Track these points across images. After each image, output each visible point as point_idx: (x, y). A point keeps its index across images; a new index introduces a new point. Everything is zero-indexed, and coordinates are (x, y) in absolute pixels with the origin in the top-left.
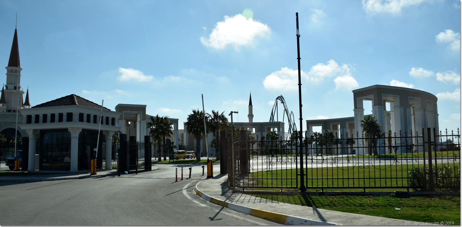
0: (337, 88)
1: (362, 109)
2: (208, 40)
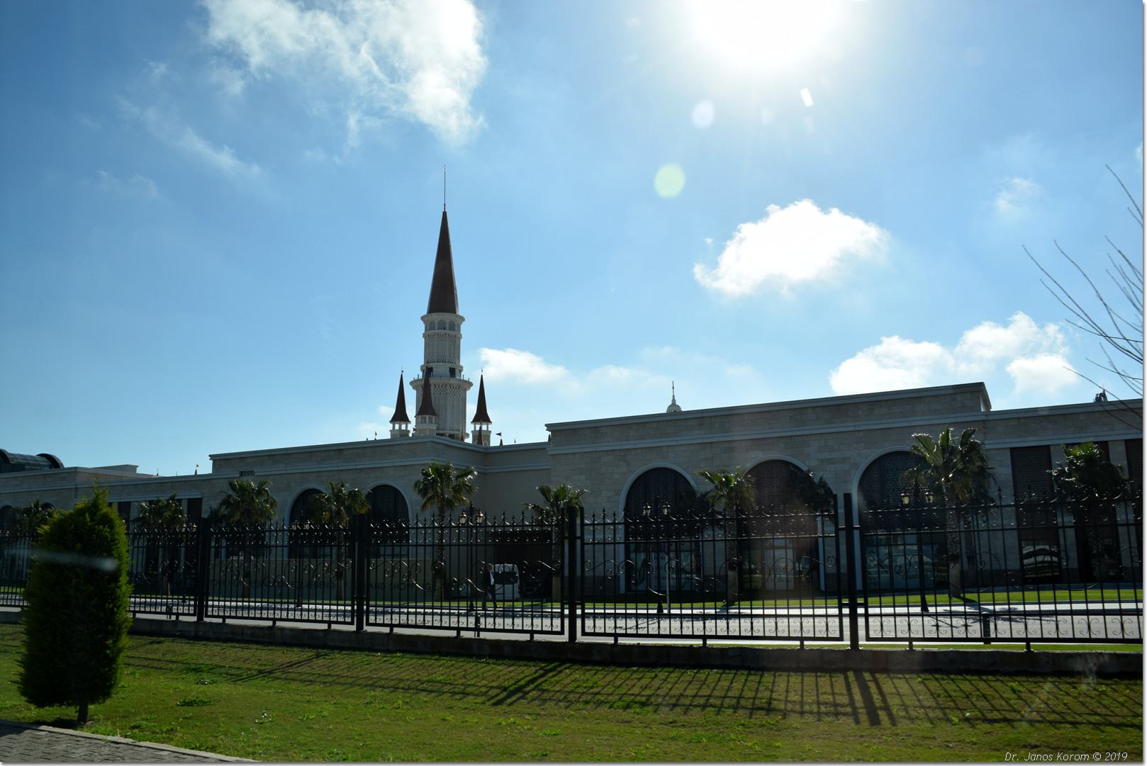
2: (714, 272)
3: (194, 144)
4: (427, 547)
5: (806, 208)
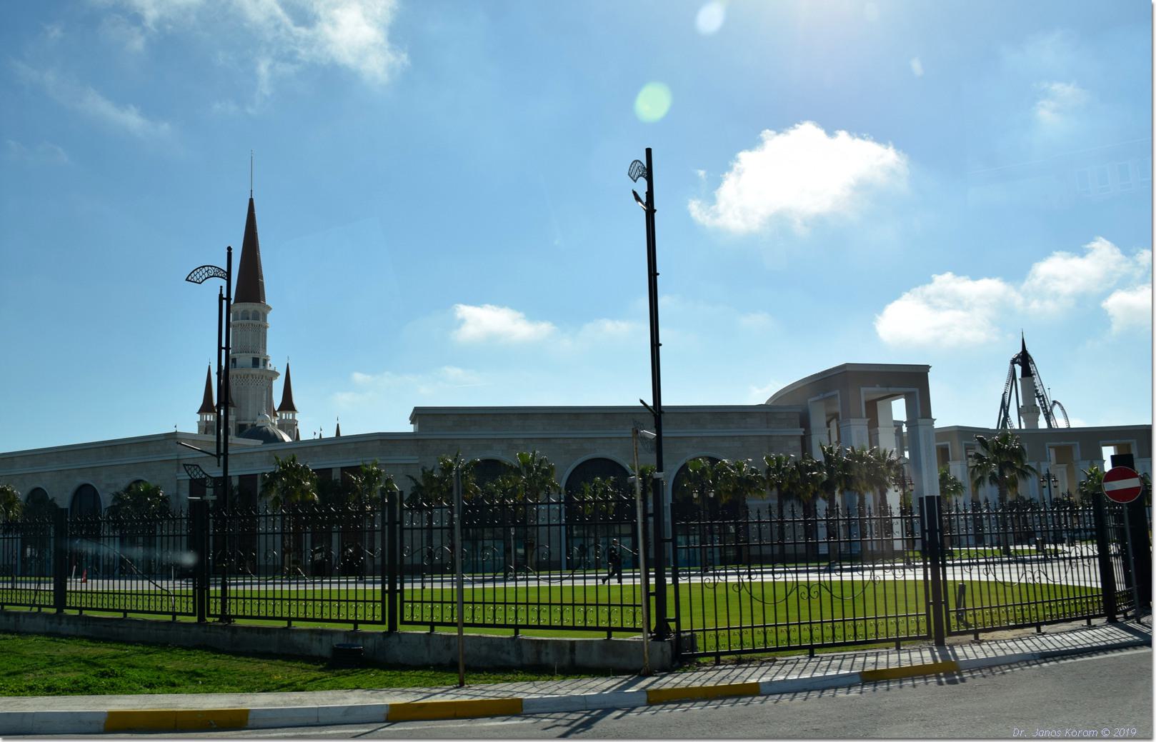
0: (1115, 328)
1: (928, 420)
2: (713, 208)
3: (100, 107)
4: (414, 531)
5: (808, 132)
